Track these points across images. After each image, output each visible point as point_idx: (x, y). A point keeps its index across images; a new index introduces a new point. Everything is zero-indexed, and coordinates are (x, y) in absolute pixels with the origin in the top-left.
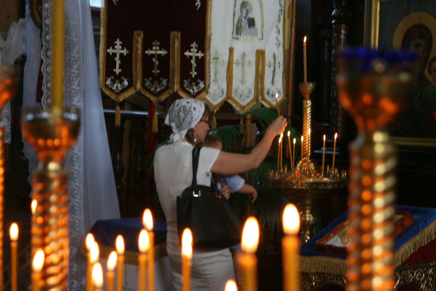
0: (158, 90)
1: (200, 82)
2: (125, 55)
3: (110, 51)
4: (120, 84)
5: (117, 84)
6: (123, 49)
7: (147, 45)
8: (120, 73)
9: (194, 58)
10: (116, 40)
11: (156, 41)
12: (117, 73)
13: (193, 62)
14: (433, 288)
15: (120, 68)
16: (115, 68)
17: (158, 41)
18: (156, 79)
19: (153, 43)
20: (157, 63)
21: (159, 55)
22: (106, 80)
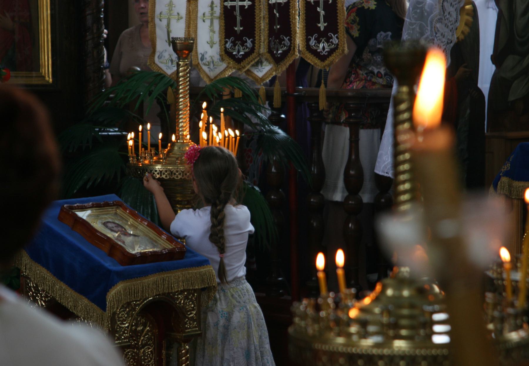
9: (238, 9)
18: (324, 36)
22: (226, 42)
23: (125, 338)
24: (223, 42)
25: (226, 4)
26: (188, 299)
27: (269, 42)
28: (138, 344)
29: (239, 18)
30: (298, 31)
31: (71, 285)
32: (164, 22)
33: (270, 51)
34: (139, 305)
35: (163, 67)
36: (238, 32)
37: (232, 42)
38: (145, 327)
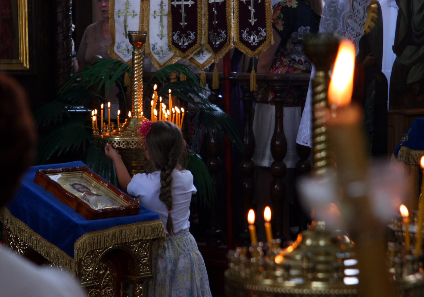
4: (257, 36)
9: (183, 7)
14: (149, 252)
15: (255, 18)
18: (254, 29)
22: (173, 35)
23: (90, 280)
24: (171, 35)
25: (173, 3)
26: (142, 247)
27: (209, 35)
28: (100, 285)
29: (184, 15)
30: (233, 25)
31: (45, 236)
32: (122, 19)
34: (101, 253)
35: (121, 55)
36: (183, 27)
37: (178, 35)
38: (106, 271)
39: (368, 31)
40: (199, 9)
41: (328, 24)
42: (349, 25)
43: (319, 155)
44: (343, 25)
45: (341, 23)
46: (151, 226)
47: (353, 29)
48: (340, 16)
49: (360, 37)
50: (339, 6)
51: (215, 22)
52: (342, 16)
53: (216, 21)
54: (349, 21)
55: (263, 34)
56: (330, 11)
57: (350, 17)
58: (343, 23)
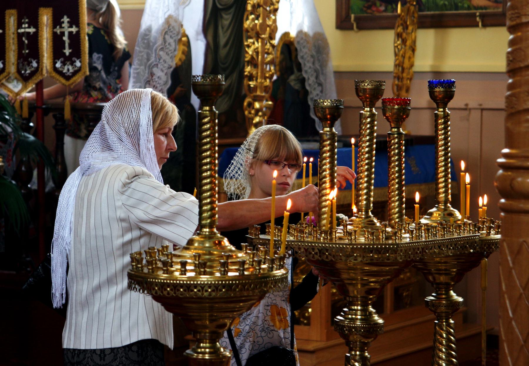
0: (28, 72)
1: (33, 60)
2: (74, 33)
3: (58, 30)
5: (68, 65)
6: (71, 27)
7: (56, 22)
8: (70, 53)
10: (63, 18)
11: (25, 17)
12: (67, 54)
13: (66, 38)
15: (70, 48)
16: (65, 49)
17: (27, 18)
18: (69, 60)
19: (23, 21)
20: (26, 42)
21: (29, 33)
27: (18, 64)
33: (19, 71)
39: (180, 63)
40: (7, 39)
41: (142, 56)
42: (161, 58)
43: (205, 188)
44: (155, 57)
45: (154, 55)
46: (414, 250)
47: (165, 61)
48: (153, 49)
49: (172, 69)
50: (152, 39)
51: (25, 51)
52: (154, 48)
53: (27, 50)
54: (161, 53)
55: (78, 64)
56: (144, 43)
57: (162, 49)
58: (156, 55)
